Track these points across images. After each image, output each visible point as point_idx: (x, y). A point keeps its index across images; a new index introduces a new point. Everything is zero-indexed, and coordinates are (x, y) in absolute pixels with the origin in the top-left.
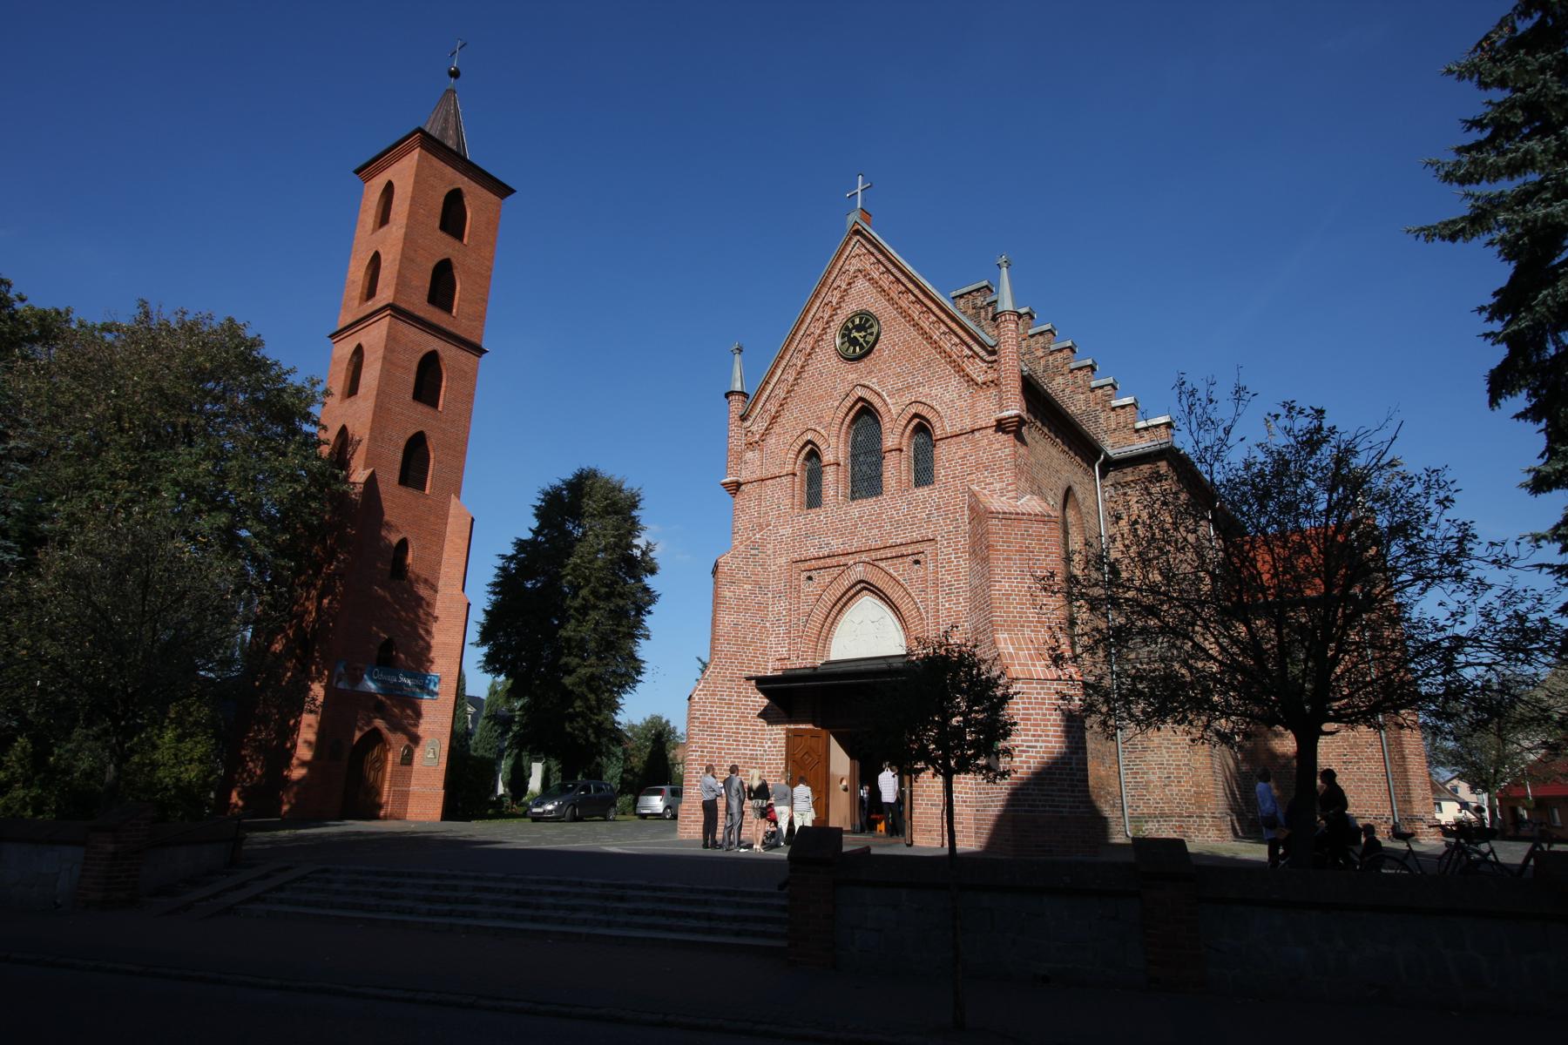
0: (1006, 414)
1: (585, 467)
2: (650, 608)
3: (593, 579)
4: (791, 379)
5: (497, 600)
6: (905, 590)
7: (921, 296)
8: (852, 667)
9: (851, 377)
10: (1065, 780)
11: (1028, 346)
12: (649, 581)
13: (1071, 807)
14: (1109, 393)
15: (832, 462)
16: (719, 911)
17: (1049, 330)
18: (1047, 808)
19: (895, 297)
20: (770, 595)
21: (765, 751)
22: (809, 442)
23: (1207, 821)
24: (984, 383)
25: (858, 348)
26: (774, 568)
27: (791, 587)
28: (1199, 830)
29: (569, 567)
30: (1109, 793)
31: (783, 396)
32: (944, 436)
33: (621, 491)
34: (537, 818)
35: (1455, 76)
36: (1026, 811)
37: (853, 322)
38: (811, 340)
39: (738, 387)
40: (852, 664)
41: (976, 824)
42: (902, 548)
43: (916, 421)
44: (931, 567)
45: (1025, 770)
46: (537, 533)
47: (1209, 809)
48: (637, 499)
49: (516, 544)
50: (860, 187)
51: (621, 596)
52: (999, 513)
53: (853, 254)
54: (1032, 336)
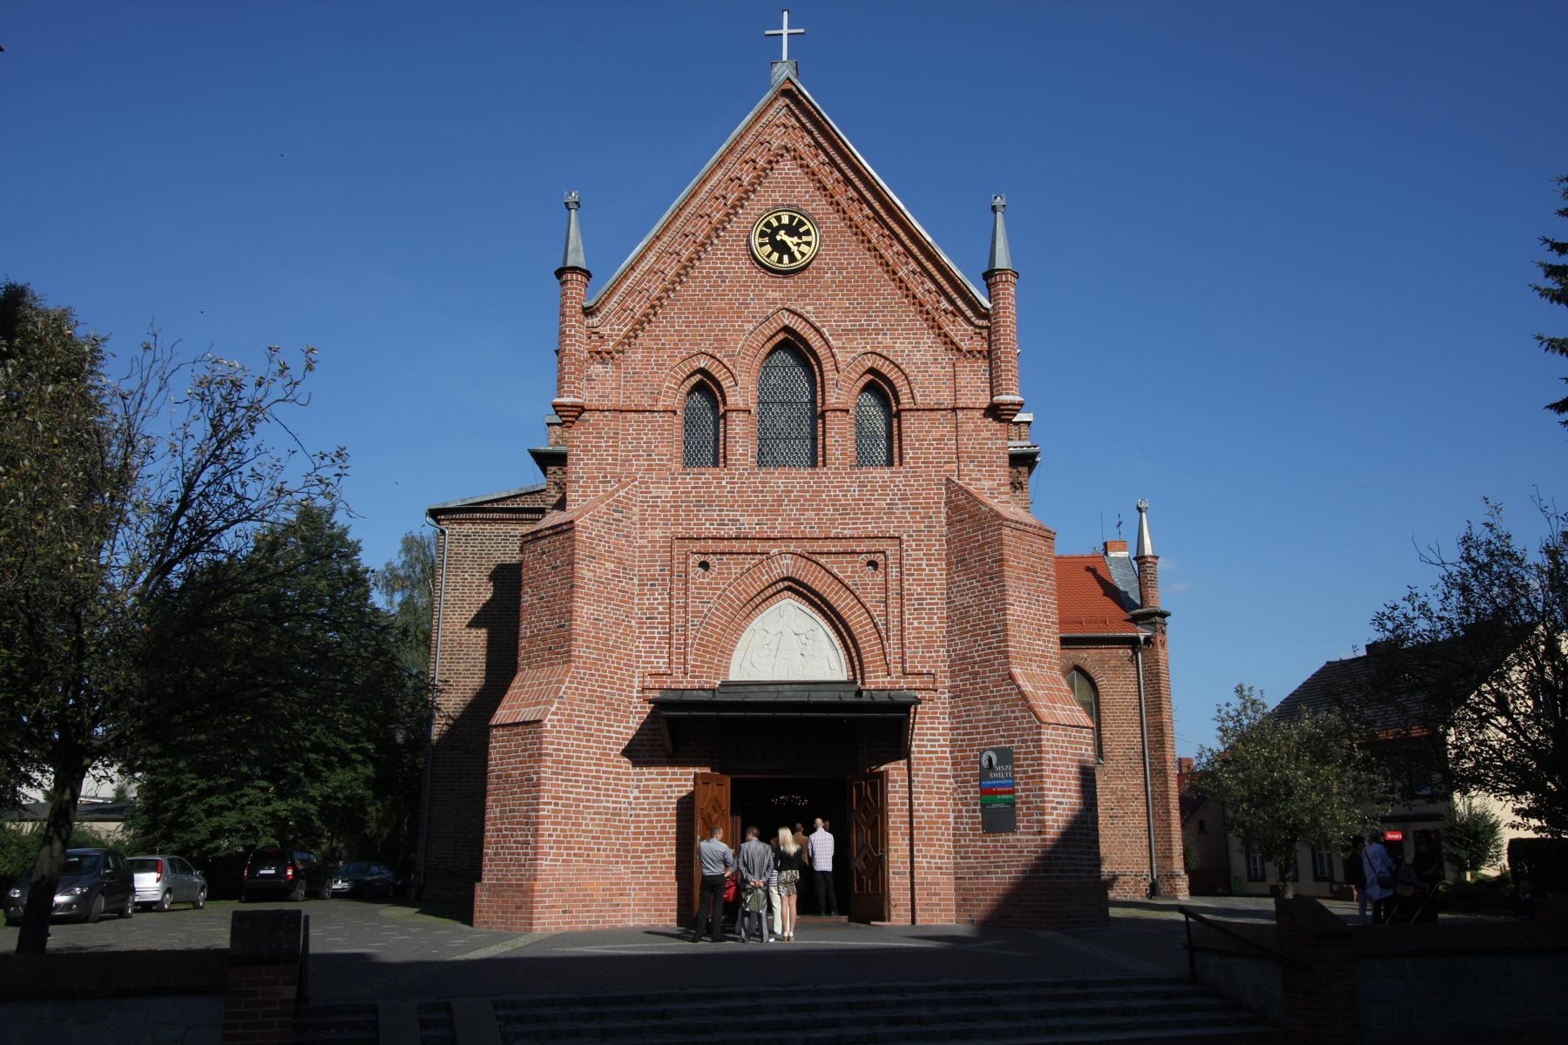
9: (771, 294)
21: (630, 803)
24: (969, 352)
25: (786, 258)
26: (644, 542)
31: (656, 294)
43: (699, 377)
44: (894, 572)
45: (1056, 830)
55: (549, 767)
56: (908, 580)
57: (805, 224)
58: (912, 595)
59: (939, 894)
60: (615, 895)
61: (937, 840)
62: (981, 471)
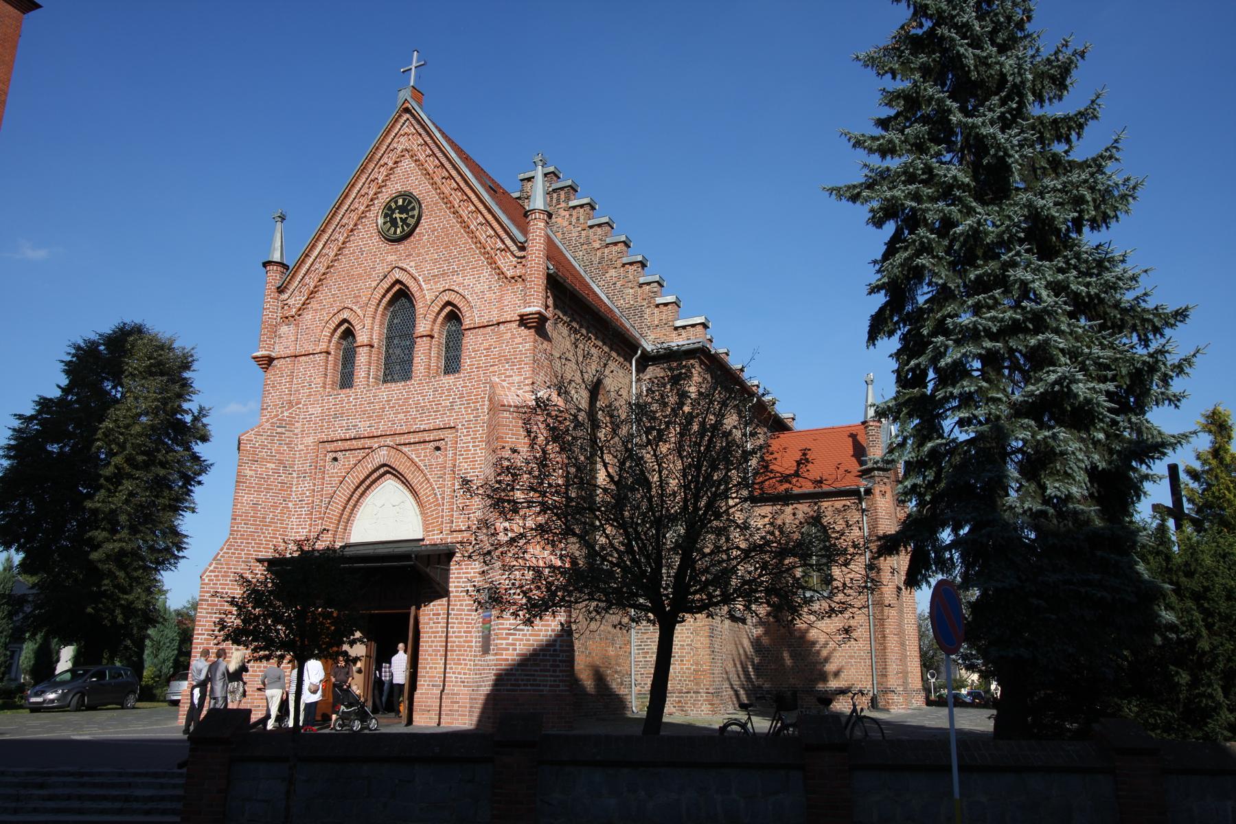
0: (528, 310)
1: (127, 321)
2: (200, 478)
3: (128, 445)
4: (332, 254)
5: (12, 465)
6: (425, 475)
7: (462, 185)
8: (369, 551)
9: (390, 258)
10: (548, 660)
11: (587, 237)
12: (200, 448)
13: (551, 686)
14: (655, 289)
15: (365, 342)
16: (138, 792)
17: (607, 223)
18: (529, 688)
19: (439, 182)
20: (295, 475)
22: (345, 321)
23: (701, 697)
24: (513, 278)
27: (316, 467)
28: (694, 705)
29: (100, 431)
30: (616, 672)
31: (323, 271)
32: (472, 326)
33: (171, 349)
34: (36, 709)
35: (862, 63)
36: (507, 690)
37: (396, 202)
38: (354, 216)
39: (276, 257)
40: (371, 547)
41: (470, 703)
42: (425, 434)
43: (449, 308)
46: (66, 390)
47: (704, 685)
48: (190, 359)
49: (38, 403)
50: (414, 64)
51: (163, 465)
52: (511, 406)
53: (402, 132)
54: (591, 227)
55: (205, 609)
56: (459, 459)
57: (412, 203)
58: (461, 470)
59: (458, 703)
60: (257, 699)
61: (464, 660)
62: (513, 369)
